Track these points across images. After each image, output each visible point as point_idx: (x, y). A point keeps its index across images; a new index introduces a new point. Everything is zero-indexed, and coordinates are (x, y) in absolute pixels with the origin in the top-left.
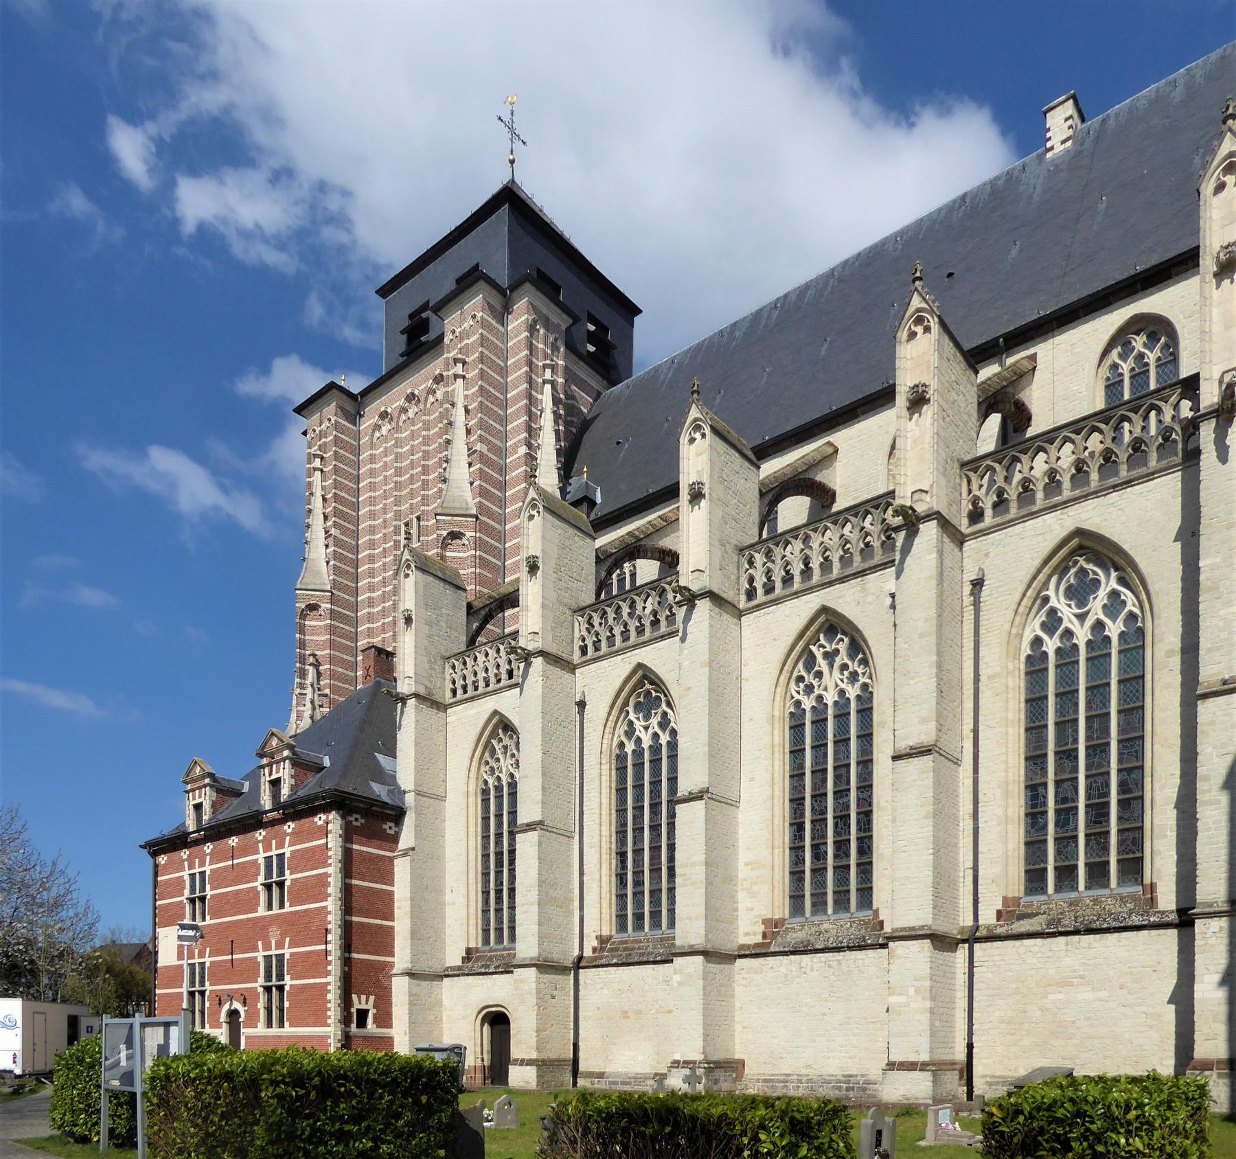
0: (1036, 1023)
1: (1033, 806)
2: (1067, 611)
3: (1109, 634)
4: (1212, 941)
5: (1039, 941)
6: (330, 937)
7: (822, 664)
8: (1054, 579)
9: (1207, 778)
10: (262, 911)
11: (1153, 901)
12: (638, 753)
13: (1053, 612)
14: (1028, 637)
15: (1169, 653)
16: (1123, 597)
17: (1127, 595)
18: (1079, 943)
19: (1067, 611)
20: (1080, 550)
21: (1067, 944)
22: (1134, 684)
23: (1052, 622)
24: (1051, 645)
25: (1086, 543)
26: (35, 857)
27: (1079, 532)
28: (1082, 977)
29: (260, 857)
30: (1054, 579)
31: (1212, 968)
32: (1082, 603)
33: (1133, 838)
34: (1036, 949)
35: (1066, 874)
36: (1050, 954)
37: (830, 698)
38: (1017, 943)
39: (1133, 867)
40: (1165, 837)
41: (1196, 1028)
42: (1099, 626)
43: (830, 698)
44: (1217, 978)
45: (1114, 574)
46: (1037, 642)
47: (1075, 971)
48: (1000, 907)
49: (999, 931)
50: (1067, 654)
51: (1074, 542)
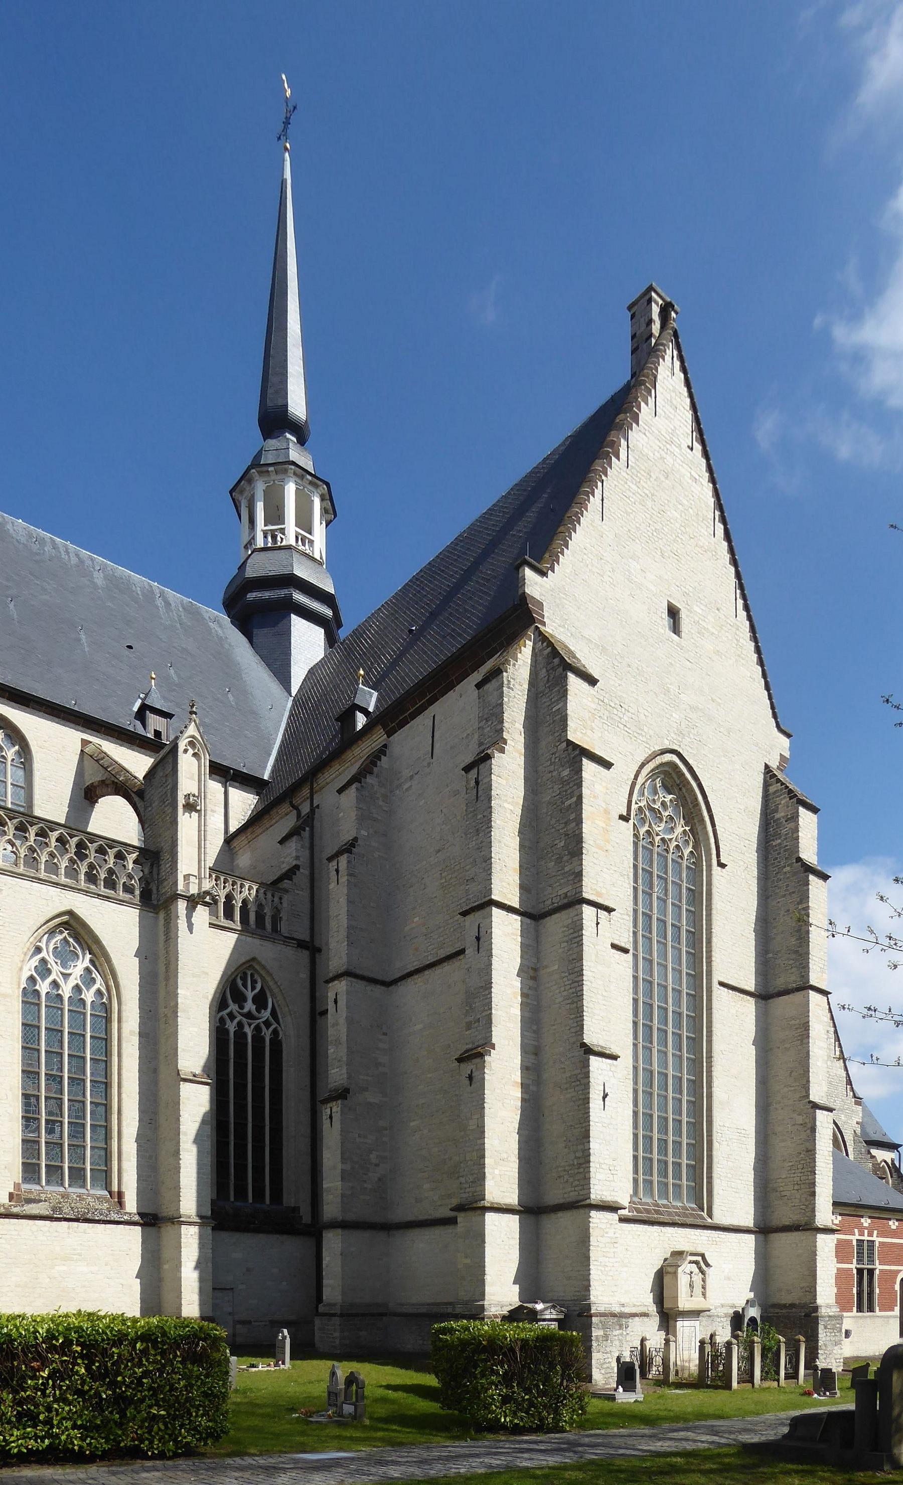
0: (46, 1289)
1: (26, 1111)
3: (39, 989)
4: (191, 1240)
5: (48, 1223)
8: (46, 936)
9: (186, 1134)
11: (121, 1204)
12: (240, 1034)
13: (43, 961)
14: (26, 974)
15: (132, 1033)
16: (94, 976)
17: (95, 974)
18: (77, 1228)
19: (56, 969)
20: (66, 925)
21: (69, 1228)
22: (104, 1042)
24: (44, 987)
25: (72, 922)
26: (470, 816)
27: (70, 913)
28: (80, 1255)
30: (46, 936)
31: (191, 1258)
33: (105, 1155)
34: (46, 1229)
35: (54, 1171)
36: (56, 1234)
38: (31, 1222)
39: (104, 1176)
40: (130, 1161)
41: (183, 1296)
42: (77, 989)
44: (193, 1264)
45: (88, 956)
46: (32, 979)
47: (75, 1250)
48: (12, 1190)
49: (15, 1210)
51: (65, 918)
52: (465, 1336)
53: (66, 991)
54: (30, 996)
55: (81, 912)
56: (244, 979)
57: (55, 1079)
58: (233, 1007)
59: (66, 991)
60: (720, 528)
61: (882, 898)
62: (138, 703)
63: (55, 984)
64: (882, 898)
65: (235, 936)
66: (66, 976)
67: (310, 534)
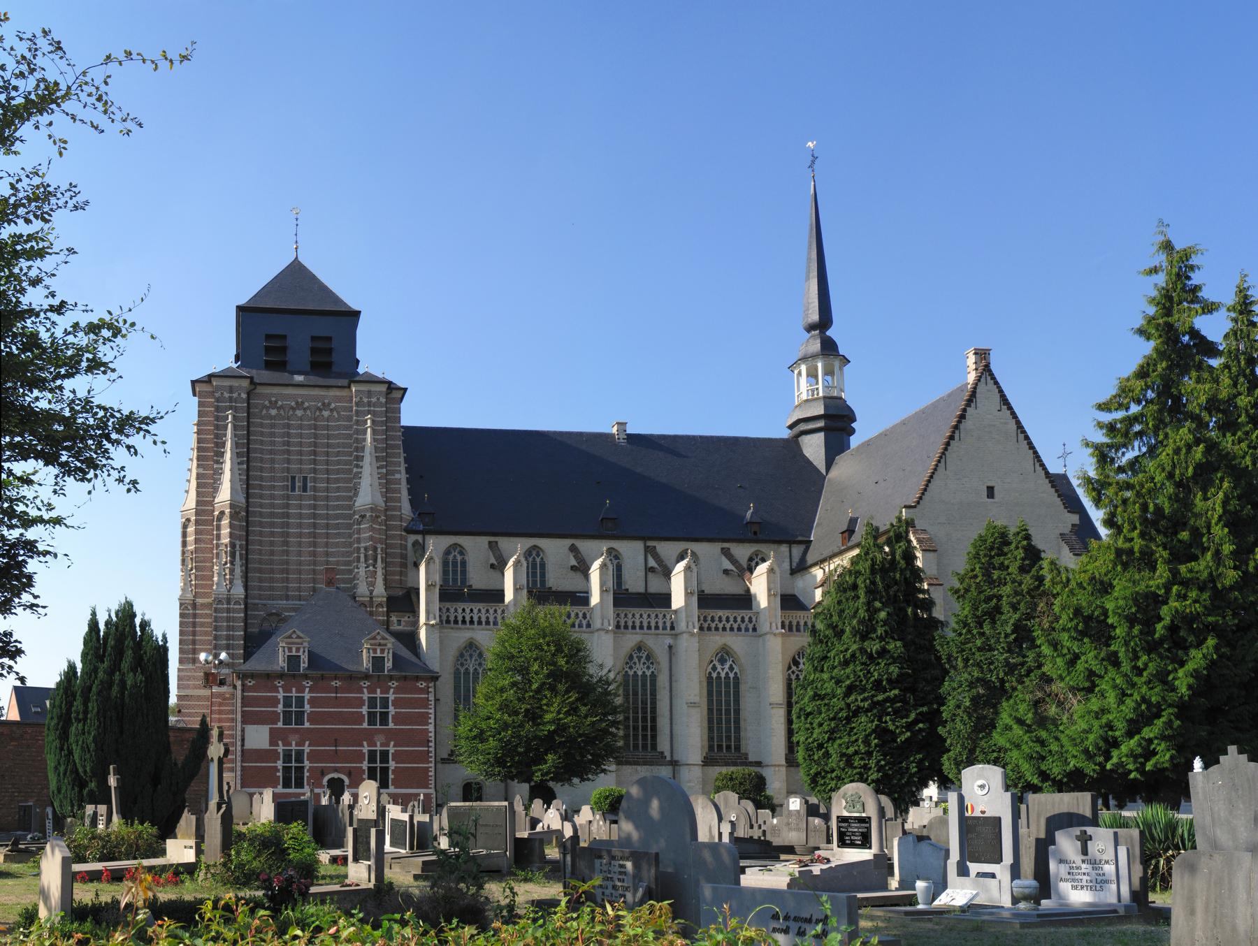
2: (719, 667)
6: (430, 744)
7: (637, 660)
10: (365, 725)
19: (719, 667)
23: (714, 668)
24: (714, 675)
29: (366, 696)
32: (722, 665)
37: (640, 673)
42: (727, 673)
43: (640, 673)
50: (719, 677)
52: (839, 570)
53: (723, 675)
54: (710, 678)
55: (729, 643)
56: (799, 655)
57: (719, 710)
58: (794, 668)
59: (723, 675)
60: (1021, 436)
61: (152, 337)
62: (972, 359)
63: (719, 673)
64: (152, 337)
65: (821, 435)
66: (723, 669)
67: (722, 549)
